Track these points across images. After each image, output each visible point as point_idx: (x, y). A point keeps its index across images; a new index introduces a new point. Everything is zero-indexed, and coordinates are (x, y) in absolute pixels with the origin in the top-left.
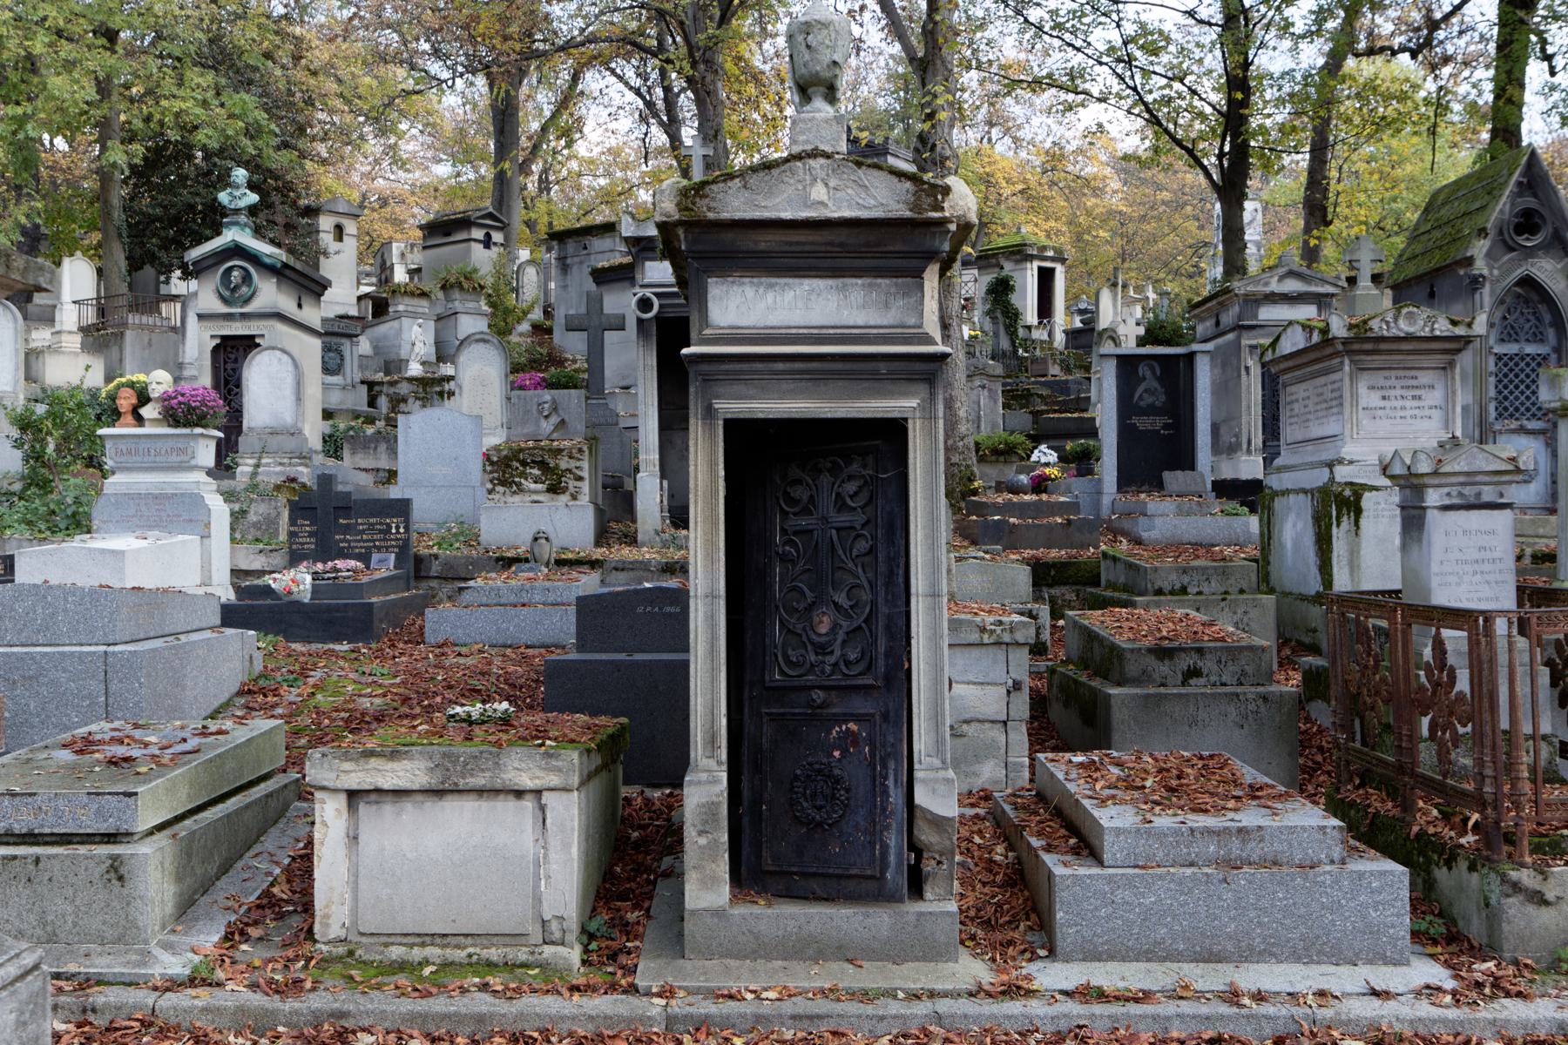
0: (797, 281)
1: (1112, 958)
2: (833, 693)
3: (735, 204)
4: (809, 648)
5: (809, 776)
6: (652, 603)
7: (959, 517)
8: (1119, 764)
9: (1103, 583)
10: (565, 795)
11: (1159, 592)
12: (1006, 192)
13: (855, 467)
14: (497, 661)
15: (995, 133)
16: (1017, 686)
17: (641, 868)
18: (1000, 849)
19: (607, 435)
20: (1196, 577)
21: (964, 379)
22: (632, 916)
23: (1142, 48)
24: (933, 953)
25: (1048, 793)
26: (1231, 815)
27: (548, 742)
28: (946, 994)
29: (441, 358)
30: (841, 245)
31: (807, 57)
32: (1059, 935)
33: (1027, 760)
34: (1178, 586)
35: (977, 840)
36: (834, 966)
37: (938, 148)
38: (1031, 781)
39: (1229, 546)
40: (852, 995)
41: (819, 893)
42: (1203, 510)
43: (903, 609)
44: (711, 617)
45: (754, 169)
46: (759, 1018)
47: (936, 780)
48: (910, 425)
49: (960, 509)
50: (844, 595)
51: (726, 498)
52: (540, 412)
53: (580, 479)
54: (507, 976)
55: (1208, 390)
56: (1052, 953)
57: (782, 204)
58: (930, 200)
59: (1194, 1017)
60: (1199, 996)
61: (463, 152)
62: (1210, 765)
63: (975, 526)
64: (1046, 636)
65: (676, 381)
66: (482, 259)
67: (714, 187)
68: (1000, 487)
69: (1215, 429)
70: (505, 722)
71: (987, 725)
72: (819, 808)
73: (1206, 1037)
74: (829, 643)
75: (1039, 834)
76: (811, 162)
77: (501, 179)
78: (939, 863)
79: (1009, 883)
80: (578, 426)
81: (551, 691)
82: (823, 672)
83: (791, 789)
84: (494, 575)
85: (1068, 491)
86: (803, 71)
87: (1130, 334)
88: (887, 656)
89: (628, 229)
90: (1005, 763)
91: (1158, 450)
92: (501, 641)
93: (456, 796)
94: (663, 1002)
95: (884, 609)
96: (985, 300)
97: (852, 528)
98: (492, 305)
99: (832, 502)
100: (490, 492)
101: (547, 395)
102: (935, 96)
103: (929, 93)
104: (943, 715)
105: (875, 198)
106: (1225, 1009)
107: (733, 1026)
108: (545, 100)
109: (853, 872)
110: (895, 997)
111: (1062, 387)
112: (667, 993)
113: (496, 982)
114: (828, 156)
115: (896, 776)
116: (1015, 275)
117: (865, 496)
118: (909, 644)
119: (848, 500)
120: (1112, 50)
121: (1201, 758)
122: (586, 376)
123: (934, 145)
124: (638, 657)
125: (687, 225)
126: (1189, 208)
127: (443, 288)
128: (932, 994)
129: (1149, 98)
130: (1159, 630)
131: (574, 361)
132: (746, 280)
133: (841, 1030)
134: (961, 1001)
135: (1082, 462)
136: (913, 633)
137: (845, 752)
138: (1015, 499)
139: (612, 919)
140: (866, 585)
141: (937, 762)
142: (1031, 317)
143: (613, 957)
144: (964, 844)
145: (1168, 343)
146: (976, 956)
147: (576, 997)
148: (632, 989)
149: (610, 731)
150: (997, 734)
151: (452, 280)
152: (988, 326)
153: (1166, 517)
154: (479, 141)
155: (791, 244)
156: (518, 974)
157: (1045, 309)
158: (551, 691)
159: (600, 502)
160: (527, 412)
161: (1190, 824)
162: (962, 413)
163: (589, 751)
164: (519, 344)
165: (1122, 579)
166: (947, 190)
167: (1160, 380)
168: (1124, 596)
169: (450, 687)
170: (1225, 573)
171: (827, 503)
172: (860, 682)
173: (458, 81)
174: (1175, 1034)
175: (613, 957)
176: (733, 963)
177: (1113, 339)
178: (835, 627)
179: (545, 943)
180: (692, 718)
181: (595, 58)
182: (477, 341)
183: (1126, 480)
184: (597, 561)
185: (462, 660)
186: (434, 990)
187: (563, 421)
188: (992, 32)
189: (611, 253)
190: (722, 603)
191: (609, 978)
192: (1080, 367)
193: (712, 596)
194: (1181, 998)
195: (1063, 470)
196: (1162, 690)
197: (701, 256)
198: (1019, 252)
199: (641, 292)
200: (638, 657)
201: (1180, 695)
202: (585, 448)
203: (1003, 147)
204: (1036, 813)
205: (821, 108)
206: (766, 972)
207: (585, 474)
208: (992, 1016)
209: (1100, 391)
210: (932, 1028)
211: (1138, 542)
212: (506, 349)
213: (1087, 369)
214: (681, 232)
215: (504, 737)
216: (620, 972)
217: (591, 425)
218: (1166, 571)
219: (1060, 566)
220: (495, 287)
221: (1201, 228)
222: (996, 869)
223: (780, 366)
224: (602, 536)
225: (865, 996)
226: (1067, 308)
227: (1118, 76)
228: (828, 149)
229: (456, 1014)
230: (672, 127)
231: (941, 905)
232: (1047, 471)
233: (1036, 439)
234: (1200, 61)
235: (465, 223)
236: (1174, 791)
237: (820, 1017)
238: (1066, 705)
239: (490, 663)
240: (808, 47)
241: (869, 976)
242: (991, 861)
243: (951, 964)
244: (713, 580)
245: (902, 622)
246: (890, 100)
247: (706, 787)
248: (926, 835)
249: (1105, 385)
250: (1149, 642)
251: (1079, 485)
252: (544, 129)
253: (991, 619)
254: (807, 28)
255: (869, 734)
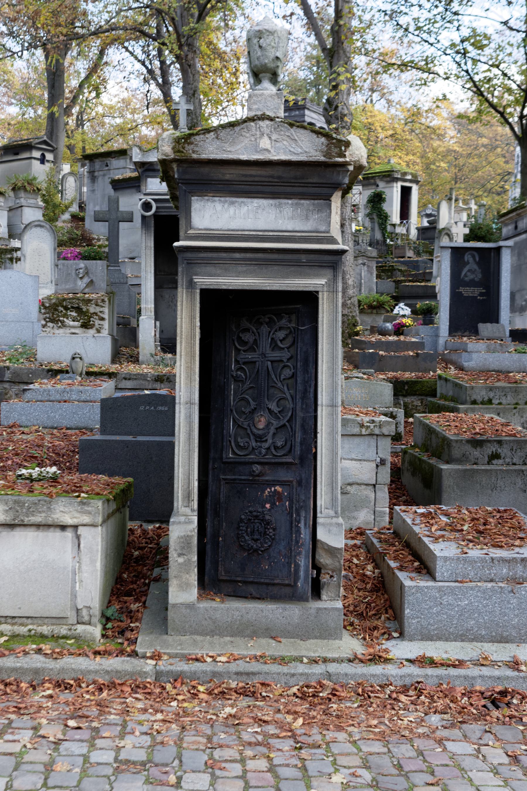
0: (249, 200)
1: (439, 639)
2: (267, 467)
3: (210, 149)
4: (252, 437)
5: (249, 520)
6: (149, 404)
7: (347, 349)
8: (447, 515)
9: (438, 395)
10: (92, 529)
11: (474, 402)
12: (381, 136)
13: (284, 322)
14: (48, 438)
15: (376, 96)
16: (383, 462)
17: (139, 576)
18: (370, 567)
19: (121, 290)
20: (498, 394)
21: (352, 259)
22: (134, 607)
23: (473, 44)
24: (326, 633)
25: (401, 532)
26: (517, 550)
27: (83, 495)
28: (333, 660)
29: (12, 235)
30: (279, 177)
31: (259, 53)
32: (406, 624)
33: (388, 509)
34: (486, 399)
35: (355, 561)
36: (264, 641)
37: (340, 109)
38: (390, 523)
39: (519, 372)
40: (275, 660)
41: (254, 594)
42: (503, 349)
43: (313, 414)
44: (189, 417)
45: (223, 127)
46: (215, 674)
47: (331, 524)
48: (320, 296)
49: (348, 344)
50: (275, 404)
51: (201, 340)
52: (77, 275)
53: (103, 319)
54: (53, 644)
55: (509, 271)
56: (402, 635)
57: (241, 150)
58: (336, 150)
59: (490, 677)
60: (494, 664)
61: (30, 100)
62: (505, 517)
63: (358, 357)
64: (401, 429)
65: (169, 261)
66: (39, 171)
67: (197, 137)
68: (373, 330)
69: (513, 296)
70: (54, 480)
71: (363, 487)
72: (256, 540)
73: (497, 690)
74: (265, 435)
75: (395, 559)
76: (261, 123)
77: (51, 117)
78: (331, 576)
79: (375, 590)
80: (102, 284)
81: (81, 459)
82: (260, 453)
83: (238, 528)
84: (46, 381)
85: (417, 334)
86: (257, 62)
87: (459, 232)
88: (301, 444)
89: (137, 156)
90: (374, 511)
91: (476, 309)
92: (50, 425)
93: (22, 528)
94: (153, 662)
95: (300, 414)
96: (366, 207)
97: (281, 361)
98: (45, 201)
99: (268, 344)
100: (44, 326)
101: (82, 264)
102: (339, 74)
103: (335, 72)
104: (337, 483)
105: (301, 148)
106: (510, 673)
107: (198, 678)
108: (82, 66)
109: (276, 581)
110: (302, 662)
111: (414, 265)
112: (156, 656)
113: (46, 648)
114: (271, 119)
115: (305, 520)
116: (386, 190)
117: (290, 340)
118: (316, 437)
119: (279, 343)
120: (453, 45)
121: (499, 511)
122: (107, 250)
123: (337, 107)
124: (140, 438)
125: (179, 162)
126: (499, 150)
127: (14, 189)
128: (325, 660)
129: (476, 78)
130: (474, 428)
131: (99, 240)
132: (217, 199)
133: (267, 682)
134: (344, 665)
135: (427, 315)
136: (319, 430)
137: (273, 505)
138: (383, 339)
139: (121, 608)
140: (289, 397)
141: (332, 513)
142: (395, 218)
143: (122, 633)
144: (347, 564)
145: (485, 241)
146: (353, 636)
147: (98, 658)
148: (134, 654)
149: (122, 487)
150: (369, 493)
151: (20, 184)
152: (368, 224)
153: (479, 353)
154: (38, 92)
155: (246, 176)
156: (60, 643)
157: (405, 214)
158: (81, 459)
159: (115, 334)
160: (69, 274)
161: (491, 555)
162: (350, 282)
163: (108, 501)
164: (63, 228)
165: (451, 393)
166: (348, 144)
167: (478, 264)
168: (452, 404)
169: (17, 454)
170: (516, 391)
171: (265, 345)
172: (284, 460)
173: (25, 52)
174: (478, 688)
175: (122, 633)
176: (199, 638)
177: (449, 235)
178: (268, 425)
179: (78, 623)
180: (176, 481)
181: (116, 40)
182: (36, 226)
183: (455, 328)
184: (113, 373)
185: (24, 437)
186: (7, 653)
187: (92, 281)
188: (375, 30)
189: (123, 170)
190: (196, 408)
191: (119, 647)
192: (426, 252)
193: (190, 403)
194: (483, 665)
195: (414, 320)
196: (475, 467)
197: (187, 182)
198: (389, 176)
199: (145, 198)
200: (140, 438)
201: (486, 471)
202: (106, 299)
203: (380, 106)
204: (393, 545)
205: (267, 88)
206: (220, 644)
207: (106, 316)
208: (363, 675)
209: (439, 268)
210: (324, 682)
211: (461, 368)
212: (54, 231)
213: (431, 253)
214: (175, 166)
215: (55, 491)
216: (126, 643)
217: (110, 284)
218: (479, 388)
219: (411, 383)
220: (48, 190)
221: (507, 162)
222: (367, 580)
223: (237, 255)
224: (116, 356)
225: (282, 661)
226: (419, 213)
227: (457, 63)
228: (272, 114)
229: (20, 668)
230: (165, 87)
231: (332, 603)
232: (404, 320)
233: (397, 299)
234: (510, 54)
235: (28, 147)
236: (481, 534)
237: (254, 674)
238: (413, 474)
239: (43, 439)
240: (260, 47)
241: (285, 648)
242: (364, 575)
243: (337, 641)
244: (191, 393)
245: (312, 423)
246: (307, 73)
247: (183, 526)
248: (323, 559)
249: (443, 267)
250: (467, 436)
251: (425, 331)
252: (81, 86)
253: (367, 419)
254: (260, 34)
255: (289, 494)
